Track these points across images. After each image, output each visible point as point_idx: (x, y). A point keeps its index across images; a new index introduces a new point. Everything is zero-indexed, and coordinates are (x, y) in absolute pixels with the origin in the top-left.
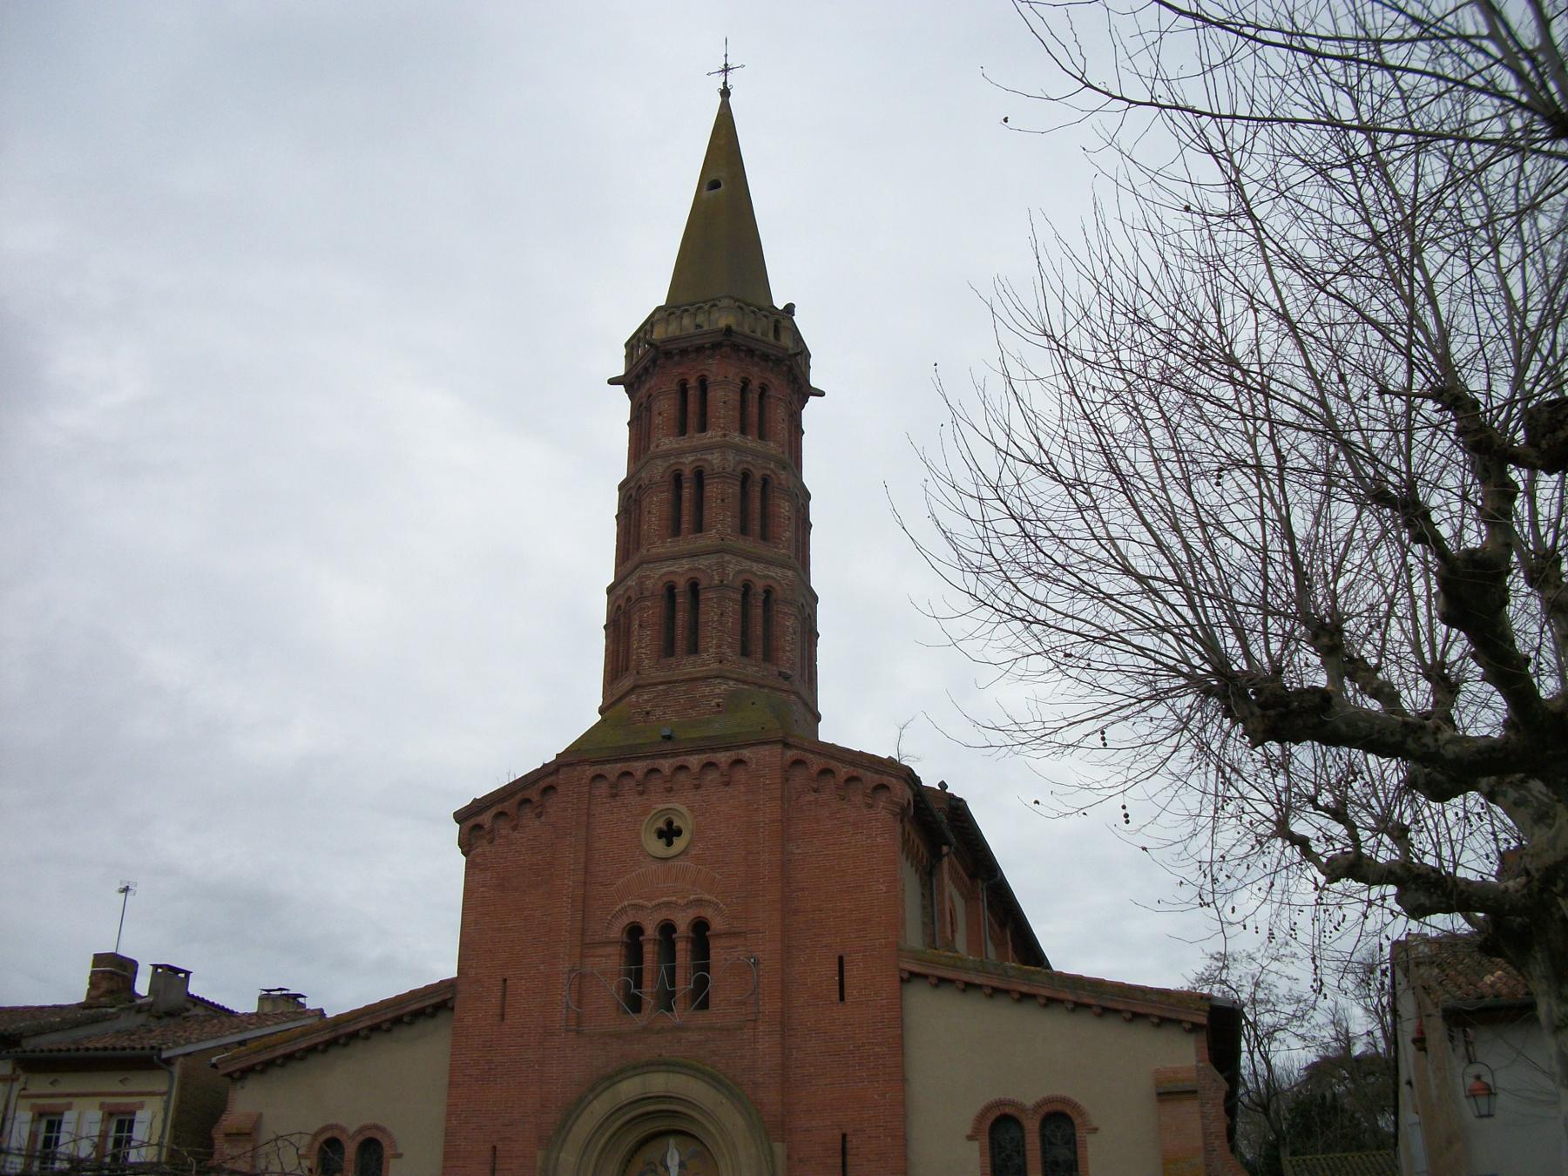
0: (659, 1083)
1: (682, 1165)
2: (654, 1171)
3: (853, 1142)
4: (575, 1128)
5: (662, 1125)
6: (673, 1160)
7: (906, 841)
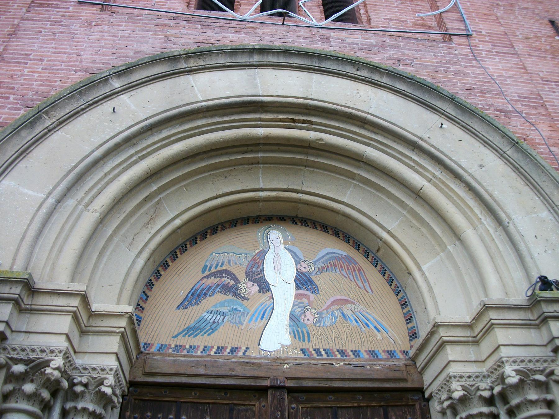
1: (303, 281)
2: (232, 290)
5: (265, 184)
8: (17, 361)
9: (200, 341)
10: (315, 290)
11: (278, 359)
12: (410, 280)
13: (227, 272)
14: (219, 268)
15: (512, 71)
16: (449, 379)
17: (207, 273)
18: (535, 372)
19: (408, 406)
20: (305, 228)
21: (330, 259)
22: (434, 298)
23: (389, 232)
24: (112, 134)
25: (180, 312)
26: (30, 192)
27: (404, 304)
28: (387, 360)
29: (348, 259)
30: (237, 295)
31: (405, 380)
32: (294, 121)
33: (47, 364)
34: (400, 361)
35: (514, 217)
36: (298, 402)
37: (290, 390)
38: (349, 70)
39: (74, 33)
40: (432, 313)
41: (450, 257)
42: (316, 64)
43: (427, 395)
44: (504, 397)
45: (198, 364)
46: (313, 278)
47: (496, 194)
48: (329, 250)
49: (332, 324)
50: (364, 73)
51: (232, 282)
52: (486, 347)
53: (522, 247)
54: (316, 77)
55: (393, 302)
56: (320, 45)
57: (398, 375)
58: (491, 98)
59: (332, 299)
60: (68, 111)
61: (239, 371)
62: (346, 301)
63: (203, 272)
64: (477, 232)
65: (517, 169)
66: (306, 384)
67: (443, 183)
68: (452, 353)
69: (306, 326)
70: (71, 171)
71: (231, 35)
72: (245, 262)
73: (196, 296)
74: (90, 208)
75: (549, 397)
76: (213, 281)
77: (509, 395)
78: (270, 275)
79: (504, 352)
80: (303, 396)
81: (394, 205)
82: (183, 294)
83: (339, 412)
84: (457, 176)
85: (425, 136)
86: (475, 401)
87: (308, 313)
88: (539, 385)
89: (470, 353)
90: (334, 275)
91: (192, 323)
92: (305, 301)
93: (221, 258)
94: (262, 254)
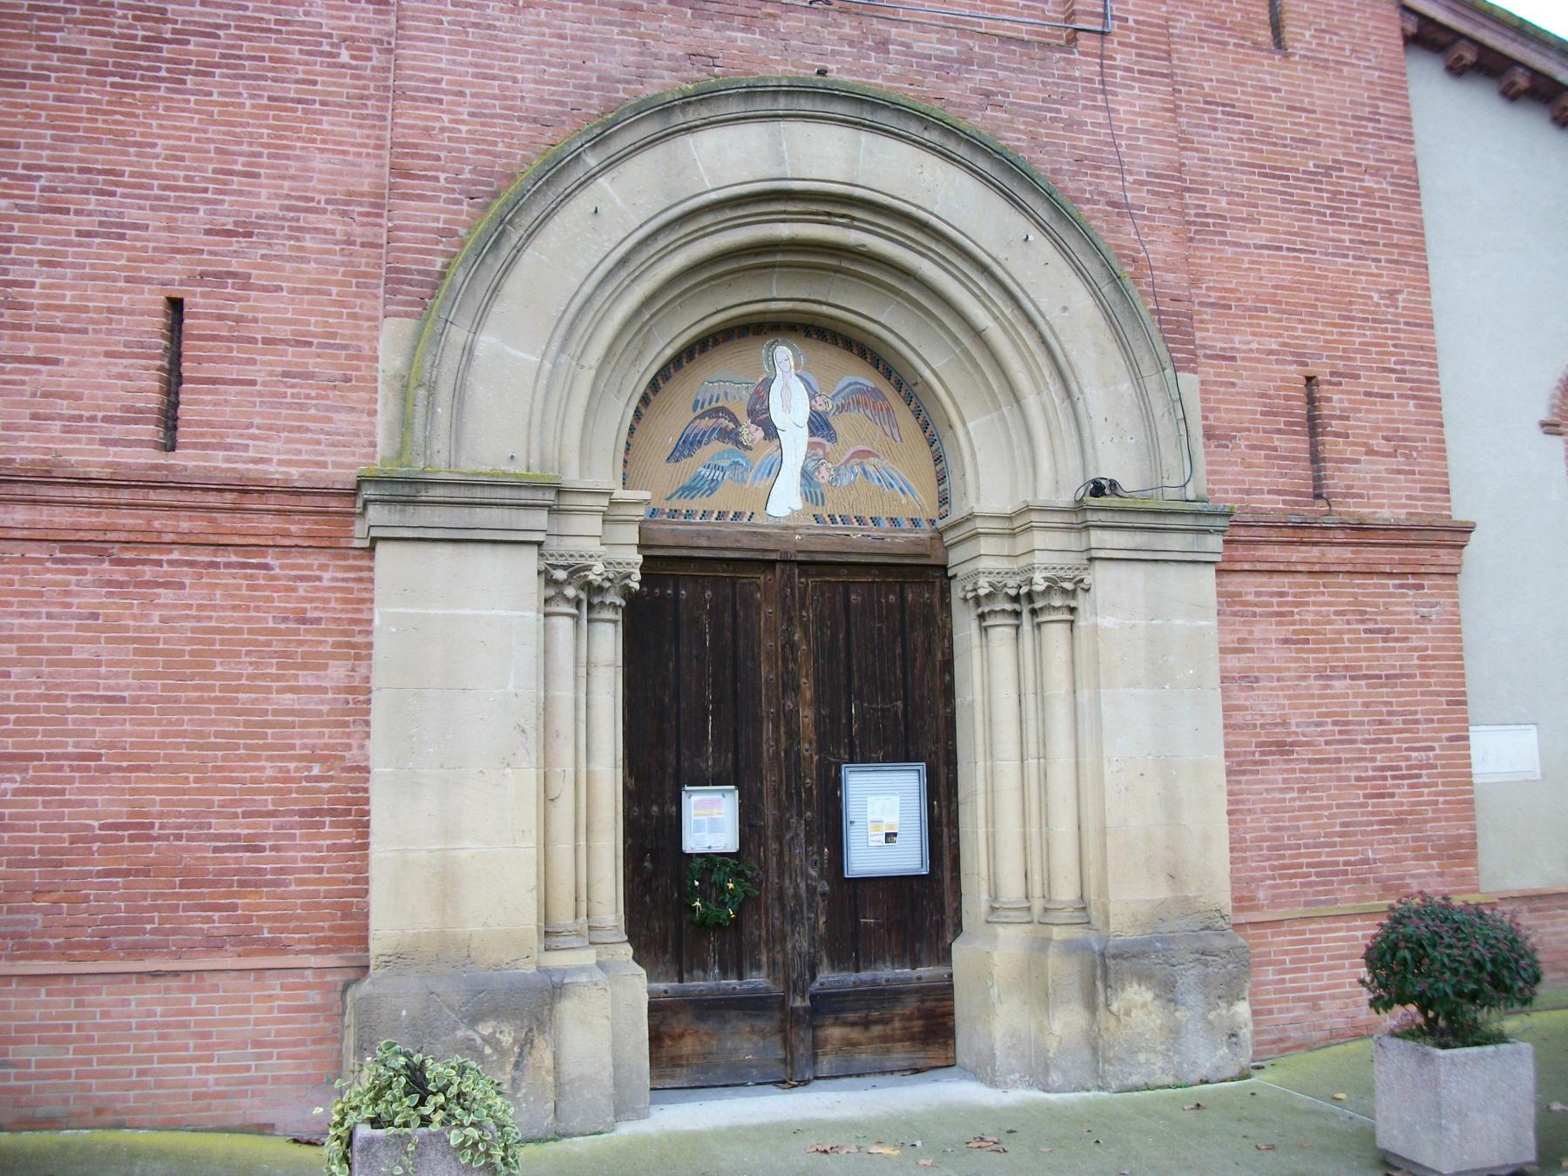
0: (824, 154)
1: (819, 425)
2: (731, 436)
3: (1335, 400)
4: (529, 257)
5: (780, 294)
6: (791, 405)
7: (1507, 1166)
8: (555, 567)
9: (698, 504)
10: (832, 437)
11: (786, 528)
12: (950, 434)
13: (722, 409)
14: (714, 405)
15: (1155, 117)
16: (977, 573)
17: (699, 411)
18: (1064, 580)
19: (927, 582)
20: (822, 344)
21: (853, 392)
22: (976, 466)
23: (933, 371)
24: (601, 256)
25: (672, 465)
26: (520, 354)
27: (938, 459)
28: (910, 531)
29: (876, 393)
30: (738, 443)
31: (928, 556)
32: (829, 214)
33: (589, 568)
34: (924, 533)
35: (1087, 390)
36: (807, 576)
37: (800, 563)
38: (914, 129)
39: (494, 27)
40: (972, 502)
41: (1002, 419)
42: (867, 115)
43: (950, 574)
44: (1030, 596)
45: (699, 534)
46: (831, 420)
47: (1073, 355)
48: (852, 379)
49: (852, 483)
50: (933, 136)
51: (732, 425)
52: (1022, 543)
53: (1086, 433)
54: (865, 137)
55: (925, 455)
56: (872, 62)
57: (921, 550)
58: (1108, 178)
59: (851, 451)
60: (535, 215)
61: (746, 542)
62: (868, 454)
63: (695, 409)
64: (1039, 398)
65: (1109, 317)
66: (818, 558)
67: (1012, 325)
68: (985, 545)
69: (819, 485)
70: (561, 319)
71: (739, 35)
72: (746, 395)
73: (688, 445)
74: (583, 362)
75: (1073, 604)
76: (707, 423)
77: (1036, 598)
78: (777, 416)
79: (1039, 558)
80: (813, 570)
81: (946, 338)
82: (672, 441)
83: (852, 588)
84: (1031, 322)
85: (1001, 257)
86: (1000, 597)
87: (823, 469)
88: (1064, 591)
89: (1003, 546)
90: (855, 415)
91: (686, 481)
92: (820, 452)
93: (716, 389)
94: (768, 383)
